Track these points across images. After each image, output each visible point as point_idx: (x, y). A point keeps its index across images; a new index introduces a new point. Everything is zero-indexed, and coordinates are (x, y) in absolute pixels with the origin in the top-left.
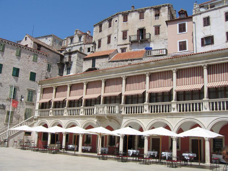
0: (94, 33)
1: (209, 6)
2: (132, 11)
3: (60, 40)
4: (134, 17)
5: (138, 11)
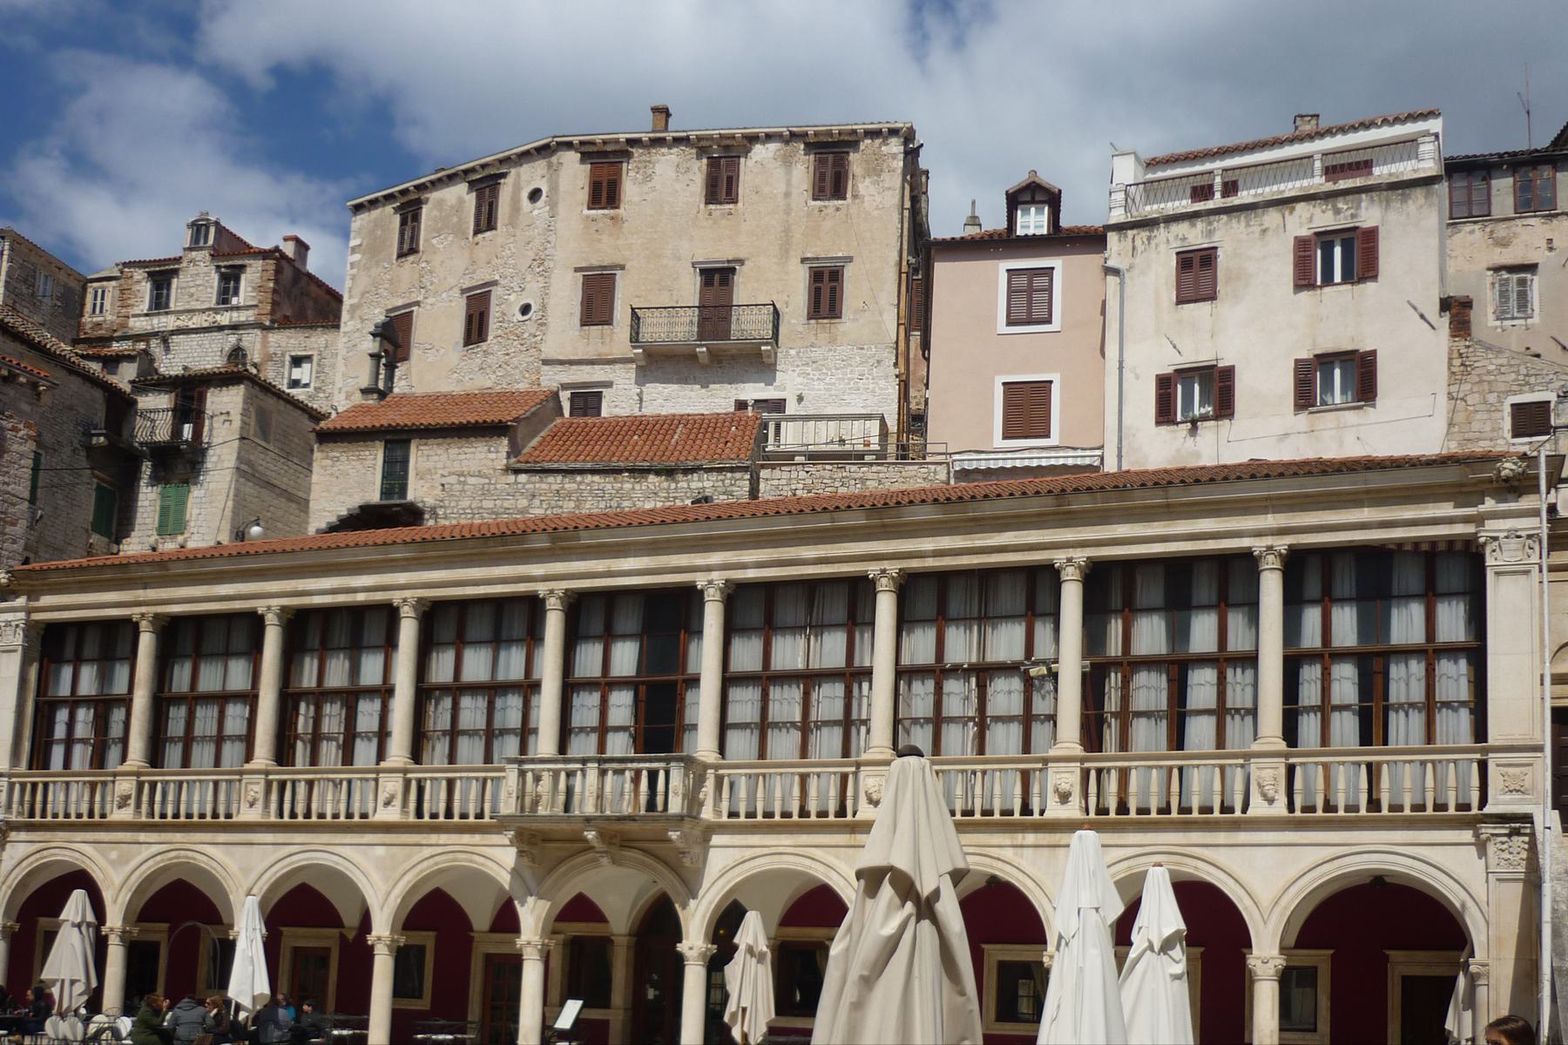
3: (62, 276)
5: (701, 146)
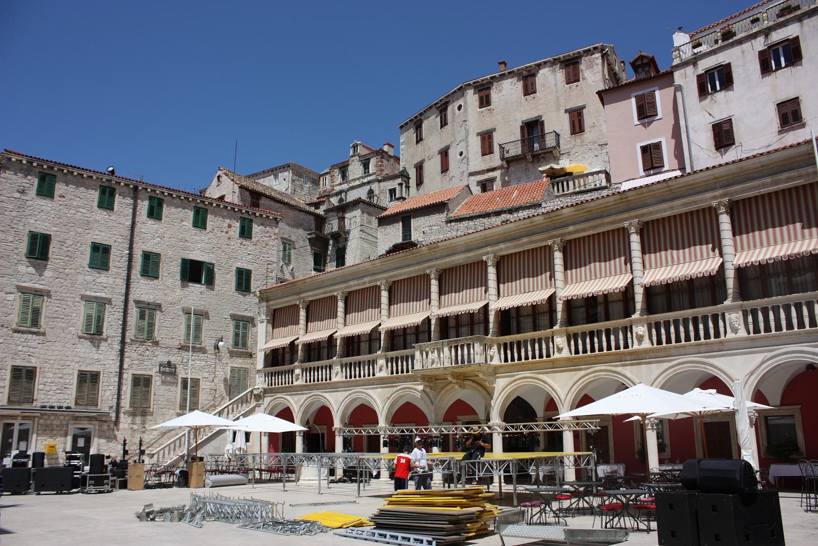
0: (402, 147)
2: (503, 77)
3: (311, 175)
4: (507, 91)
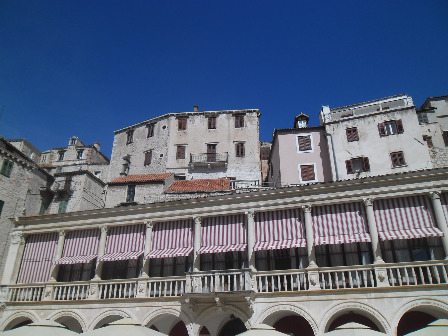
0: (114, 145)
1: (354, 111)
